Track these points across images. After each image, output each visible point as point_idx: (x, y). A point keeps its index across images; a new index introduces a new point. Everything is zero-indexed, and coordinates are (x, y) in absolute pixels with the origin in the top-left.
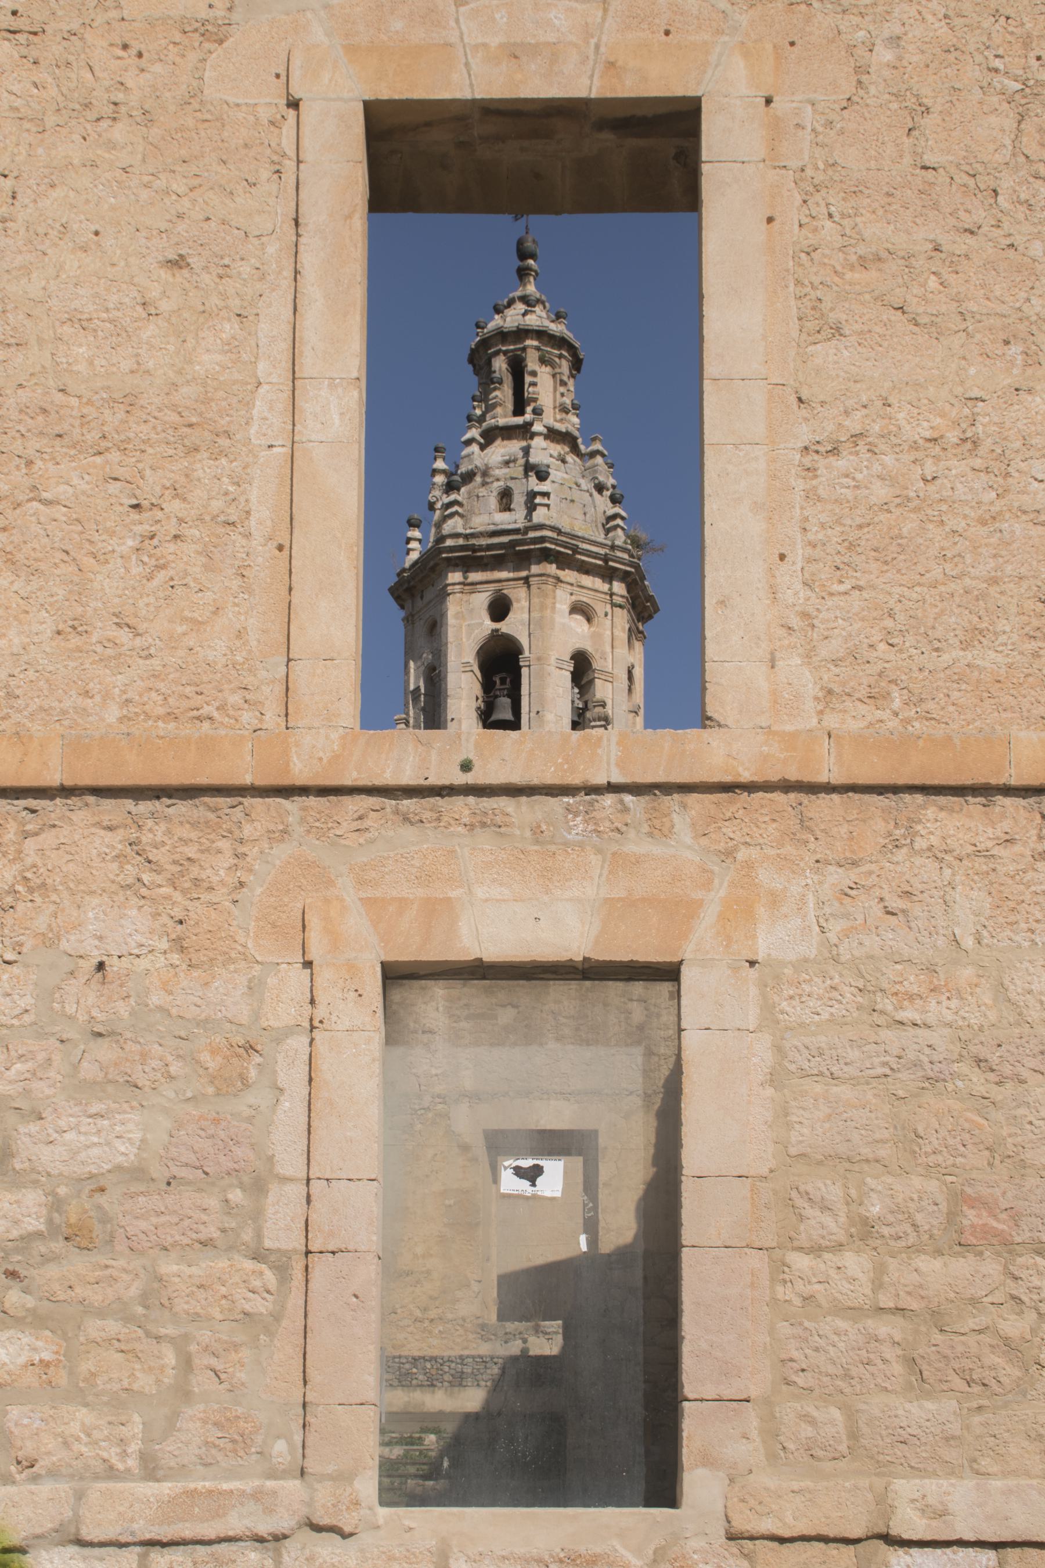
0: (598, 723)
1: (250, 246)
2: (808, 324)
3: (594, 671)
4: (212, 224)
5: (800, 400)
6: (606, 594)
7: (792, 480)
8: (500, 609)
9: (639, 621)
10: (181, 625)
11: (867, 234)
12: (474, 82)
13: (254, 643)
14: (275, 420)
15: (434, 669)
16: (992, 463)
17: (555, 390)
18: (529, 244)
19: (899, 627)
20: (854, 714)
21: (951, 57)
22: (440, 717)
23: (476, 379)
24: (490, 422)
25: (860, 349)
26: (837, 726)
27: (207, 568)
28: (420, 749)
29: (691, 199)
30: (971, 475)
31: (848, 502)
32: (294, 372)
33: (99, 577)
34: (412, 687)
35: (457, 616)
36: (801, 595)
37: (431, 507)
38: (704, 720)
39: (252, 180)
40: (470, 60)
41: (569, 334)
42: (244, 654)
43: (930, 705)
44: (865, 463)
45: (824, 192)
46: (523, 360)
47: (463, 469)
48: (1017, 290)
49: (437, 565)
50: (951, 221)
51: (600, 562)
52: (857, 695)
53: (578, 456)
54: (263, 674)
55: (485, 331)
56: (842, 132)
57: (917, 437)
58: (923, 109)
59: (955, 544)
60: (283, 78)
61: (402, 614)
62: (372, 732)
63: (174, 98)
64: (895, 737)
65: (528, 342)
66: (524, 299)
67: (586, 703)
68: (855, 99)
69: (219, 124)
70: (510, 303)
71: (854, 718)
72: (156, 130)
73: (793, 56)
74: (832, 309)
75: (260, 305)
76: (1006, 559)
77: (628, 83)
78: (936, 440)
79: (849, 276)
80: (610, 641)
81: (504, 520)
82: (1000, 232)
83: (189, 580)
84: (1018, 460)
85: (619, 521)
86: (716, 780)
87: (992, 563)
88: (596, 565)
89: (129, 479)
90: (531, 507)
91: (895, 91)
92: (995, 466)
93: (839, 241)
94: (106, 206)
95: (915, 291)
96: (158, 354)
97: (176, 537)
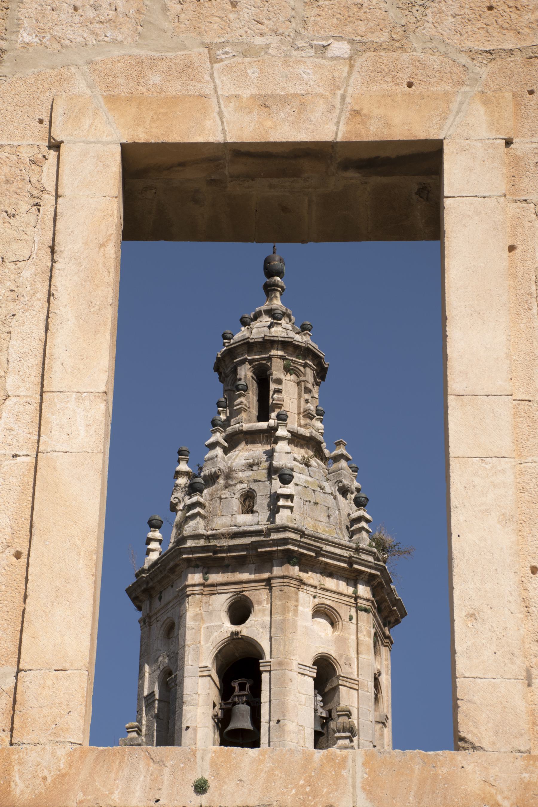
0: (343, 734)
1: (6, 270)
3: (338, 677)
6: (350, 597)
8: (240, 611)
9: (385, 626)
12: (226, 128)
14: (21, 431)
15: (170, 673)
17: (300, 397)
18: (276, 263)
22: (174, 725)
23: (221, 385)
24: (234, 427)
28: (153, 767)
29: (434, 229)
34: (146, 693)
35: (195, 618)
37: (173, 508)
38: (458, 742)
41: (313, 344)
46: (269, 368)
47: (206, 472)
49: (176, 565)
51: (344, 565)
53: (321, 460)
55: (232, 341)
60: (46, 123)
61: (139, 615)
62: (101, 748)
65: (274, 352)
66: (270, 313)
67: (330, 712)
70: (256, 317)
73: (532, 103)
75: (12, 324)
80: (354, 645)
81: (246, 521)
85: (363, 524)
88: (340, 568)
90: (274, 509)
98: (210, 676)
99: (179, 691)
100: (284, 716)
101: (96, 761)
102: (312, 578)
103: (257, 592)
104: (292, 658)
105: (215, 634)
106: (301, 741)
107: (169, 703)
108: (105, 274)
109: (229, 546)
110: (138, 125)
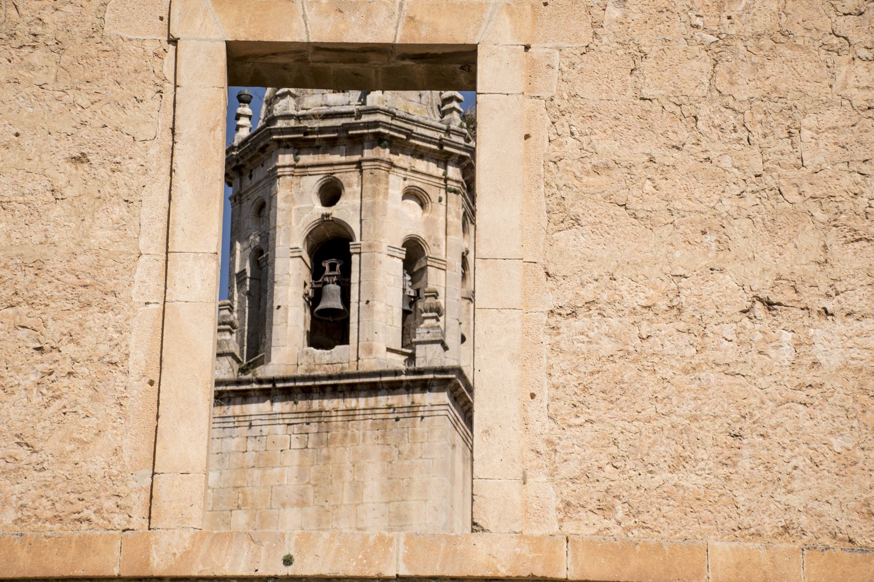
0: (430, 314)
1: (137, 148)
2: (555, 216)
3: (426, 258)
4: (108, 130)
5: (547, 273)
6: (440, 178)
7: (541, 336)
8: (331, 193)
10: (70, 444)
11: (599, 148)
13: (127, 459)
15: (261, 252)
16: (692, 326)
19: (621, 453)
20: (587, 522)
21: (663, 16)
22: (266, 304)
25: (593, 236)
26: (574, 532)
27: (93, 399)
28: (253, 546)
30: (676, 334)
31: (583, 354)
32: (167, 247)
33: (6, 405)
34: (237, 270)
35: (287, 199)
36: (547, 426)
39: (139, 97)
40: (307, 13)
42: (119, 468)
43: (645, 517)
44: (596, 324)
45: (567, 116)
48: (712, 193)
49: (267, 146)
50: (663, 140)
52: (589, 507)
54: (132, 484)
56: (581, 72)
57: (635, 305)
58: (642, 55)
59: (665, 388)
60: (166, 20)
63: (81, 32)
64: (618, 543)
67: (418, 291)
68: (592, 46)
69: (115, 54)
71: (586, 526)
72: (67, 57)
73: (546, 13)
74: (573, 205)
76: (703, 401)
77: (424, 33)
78: (650, 307)
79: (585, 179)
82: (698, 148)
83: (77, 408)
84: (712, 324)
85: (455, 104)
86: (480, 574)
87: (693, 404)
88: (430, 150)
89: (35, 327)
91: (621, 41)
92: (695, 328)
93: (578, 154)
94: (25, 114)
95: (635, 193)
96: (63, 229)
97: (69, 373)
98: (301, 257)
99: (270, 271)
100: (373, 297)
101: (212, 541)
102: (402, 160)
103: (348, 174)
104: (382, 240)
105: (306, 216)
106: (390, 320)
107: (260, 280)
108: (215, 154)
109: (320, 128)
110: (239, 25)
